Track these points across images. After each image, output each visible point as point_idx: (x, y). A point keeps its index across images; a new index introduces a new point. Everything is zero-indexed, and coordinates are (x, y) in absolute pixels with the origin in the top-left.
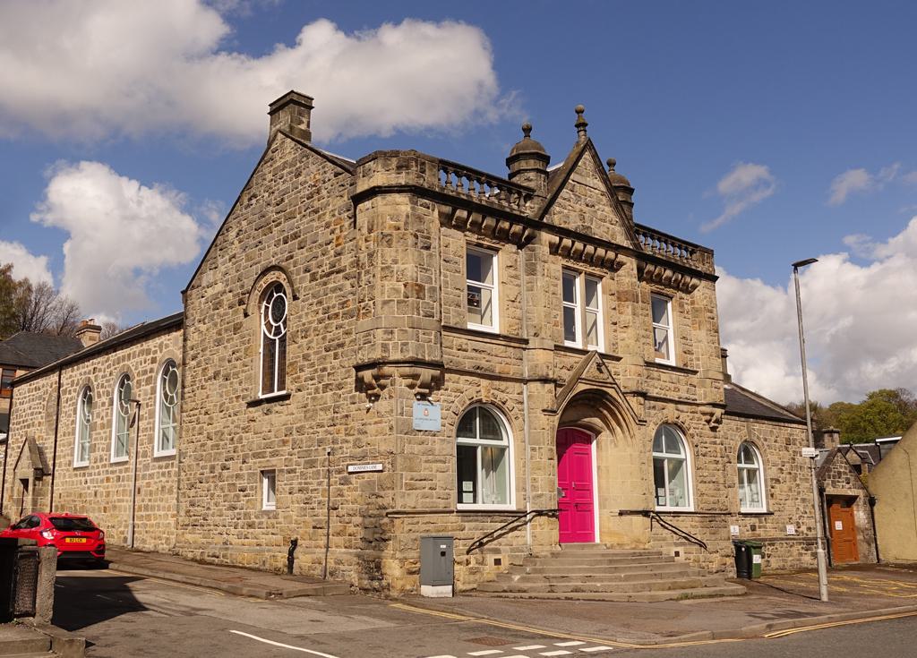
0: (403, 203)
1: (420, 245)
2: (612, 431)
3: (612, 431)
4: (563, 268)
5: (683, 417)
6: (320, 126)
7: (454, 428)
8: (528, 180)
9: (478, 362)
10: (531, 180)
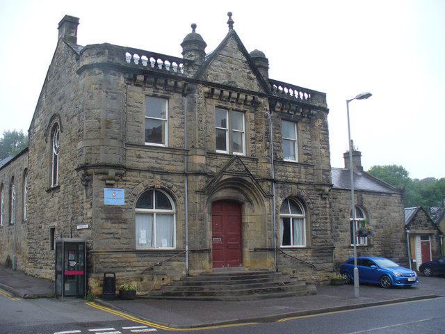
0: (99, 76)
1: (109, 97)
2: (251, 202)
3: (251, 202)
4: (216, 107)
5: (303, 193)
6: (84, 38)
7: (136, 200)
8: (191, 56)
9: (152, 165)
10: (192, 56)
